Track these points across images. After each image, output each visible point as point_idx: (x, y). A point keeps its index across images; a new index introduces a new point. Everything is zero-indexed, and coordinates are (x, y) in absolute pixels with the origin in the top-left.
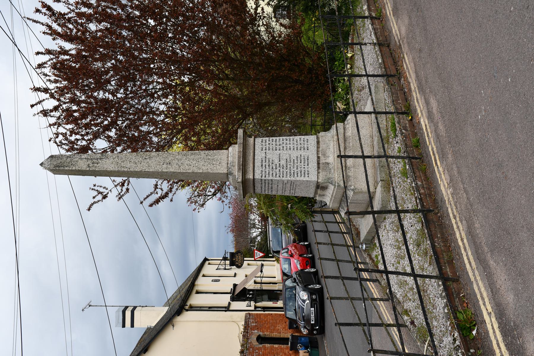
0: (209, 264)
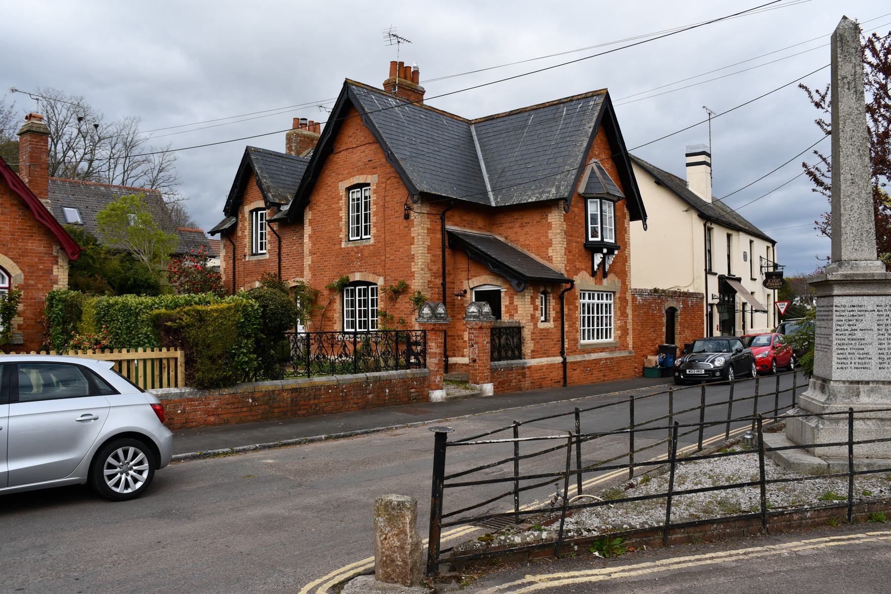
0: (768, 247)
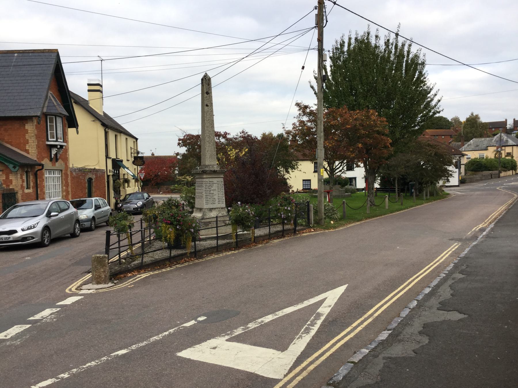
0: (134, 142)
